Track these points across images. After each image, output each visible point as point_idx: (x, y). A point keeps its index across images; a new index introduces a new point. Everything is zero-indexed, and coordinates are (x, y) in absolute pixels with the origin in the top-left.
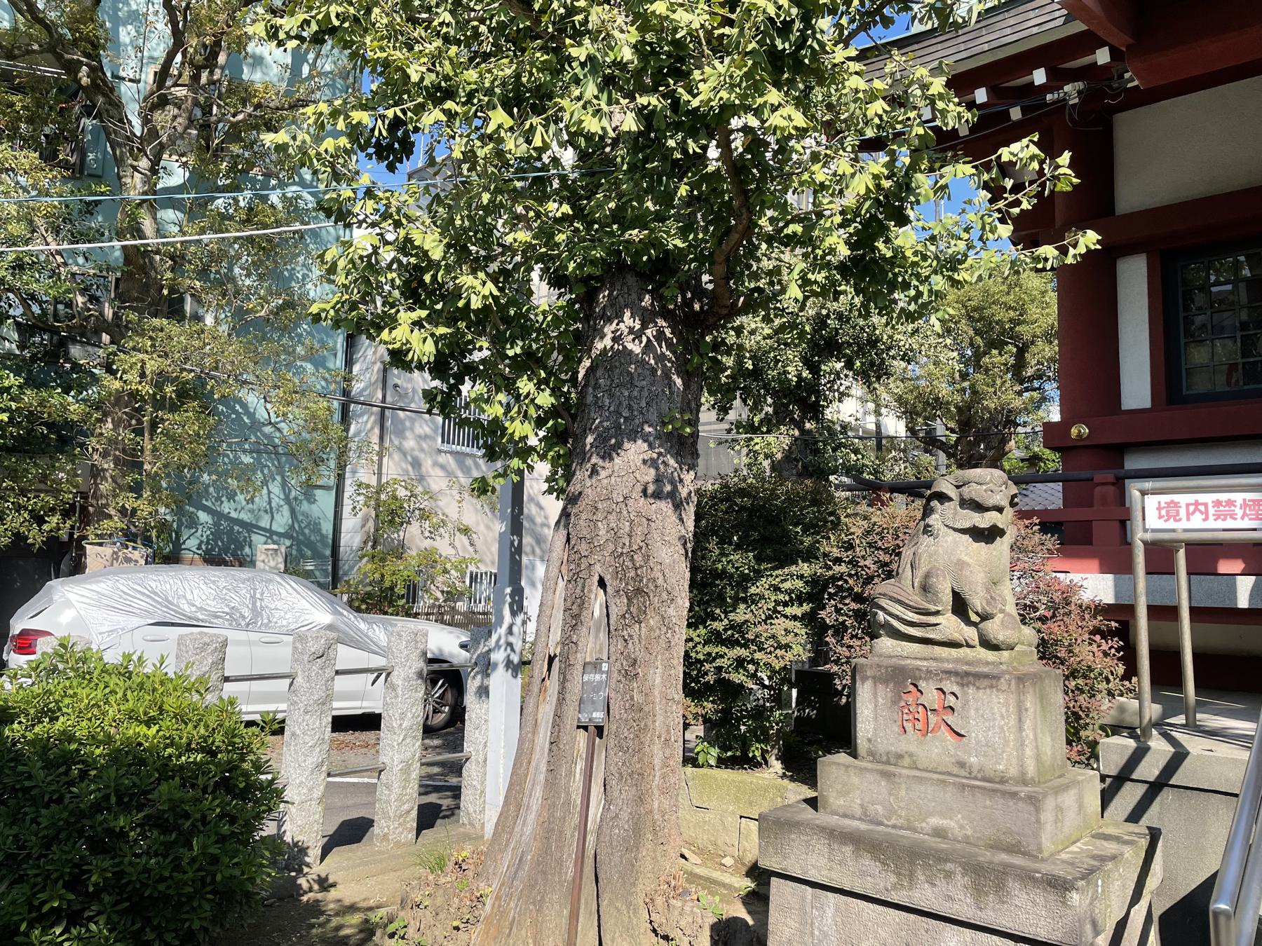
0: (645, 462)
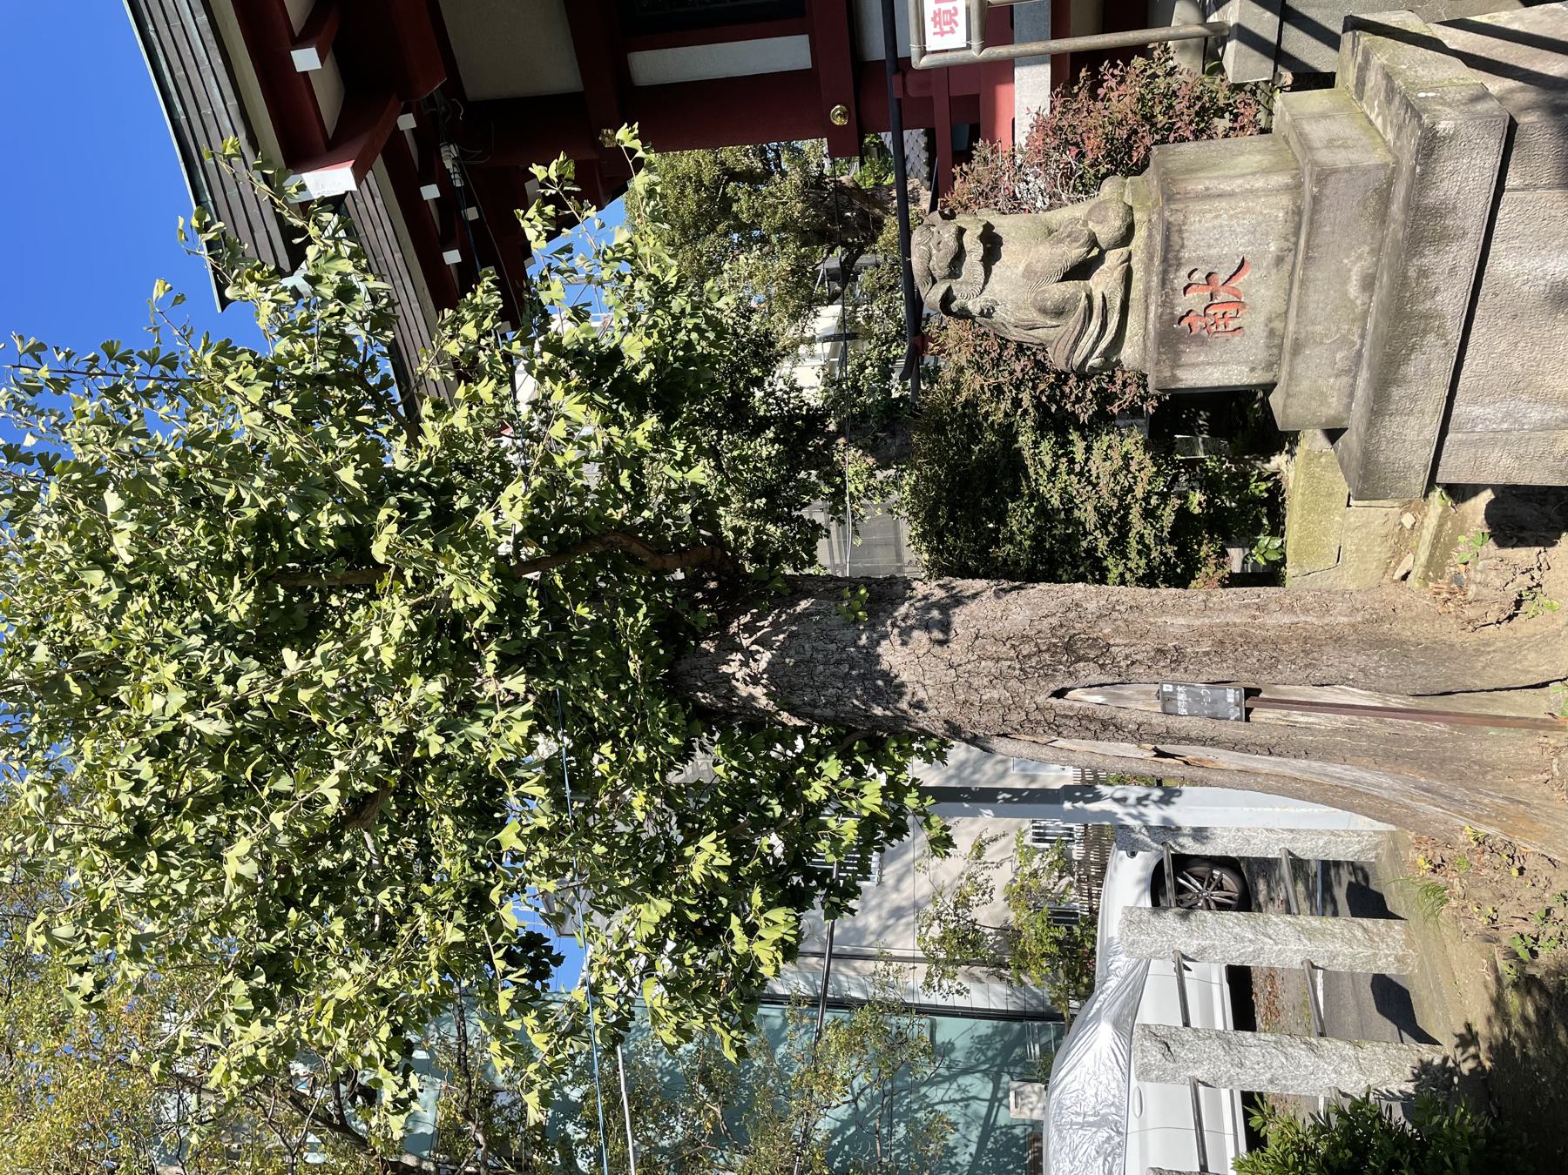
0: (904, 643)
